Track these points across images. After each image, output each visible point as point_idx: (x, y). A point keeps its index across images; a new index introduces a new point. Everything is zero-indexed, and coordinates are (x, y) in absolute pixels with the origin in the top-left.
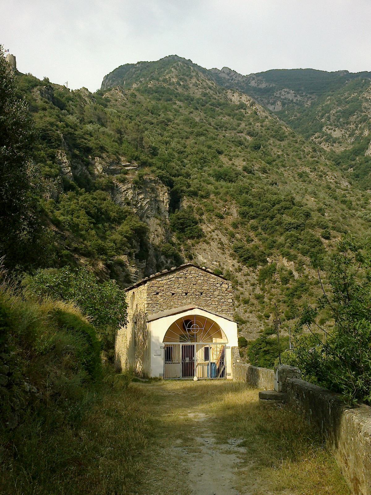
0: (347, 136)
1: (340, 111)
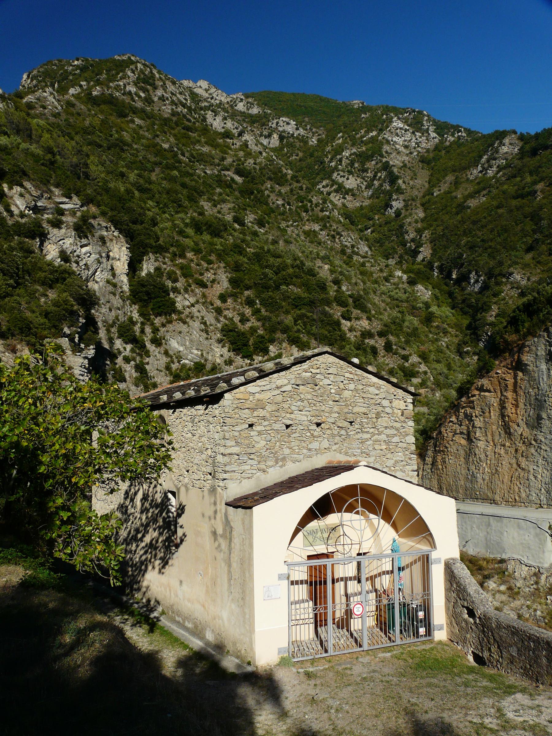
0: (364, 187)
1: (354, 154)
